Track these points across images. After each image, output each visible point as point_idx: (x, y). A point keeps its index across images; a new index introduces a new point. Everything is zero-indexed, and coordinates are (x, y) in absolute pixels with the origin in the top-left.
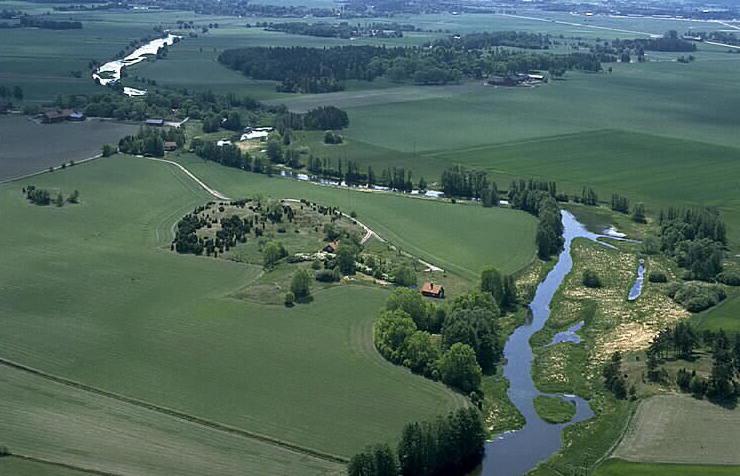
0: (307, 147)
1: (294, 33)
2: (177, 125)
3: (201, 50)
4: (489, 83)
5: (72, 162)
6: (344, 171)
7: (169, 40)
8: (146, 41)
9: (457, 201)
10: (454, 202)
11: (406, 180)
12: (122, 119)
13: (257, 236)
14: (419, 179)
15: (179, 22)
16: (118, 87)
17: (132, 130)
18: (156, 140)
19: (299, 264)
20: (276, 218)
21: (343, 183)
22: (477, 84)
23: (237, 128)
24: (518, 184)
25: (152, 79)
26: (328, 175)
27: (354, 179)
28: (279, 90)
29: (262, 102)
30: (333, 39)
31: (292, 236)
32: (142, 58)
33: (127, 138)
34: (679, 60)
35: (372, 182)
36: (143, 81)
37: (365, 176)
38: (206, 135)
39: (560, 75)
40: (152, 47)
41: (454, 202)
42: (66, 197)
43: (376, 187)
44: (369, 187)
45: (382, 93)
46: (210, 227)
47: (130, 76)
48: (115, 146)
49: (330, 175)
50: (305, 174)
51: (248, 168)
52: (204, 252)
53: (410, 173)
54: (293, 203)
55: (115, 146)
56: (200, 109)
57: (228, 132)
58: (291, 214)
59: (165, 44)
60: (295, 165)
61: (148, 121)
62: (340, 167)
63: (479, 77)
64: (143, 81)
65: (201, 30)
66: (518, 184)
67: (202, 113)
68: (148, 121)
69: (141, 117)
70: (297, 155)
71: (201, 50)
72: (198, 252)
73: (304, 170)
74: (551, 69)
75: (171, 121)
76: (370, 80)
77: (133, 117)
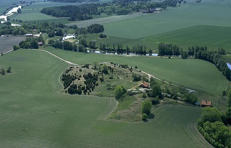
0: (95, 40)
1: (62, 2)
2: (38, 35)
3: (33, 9)
4: (142, 12)
5: (2, 54)
6: (116, 48)
7: (20, 7)
8: (12, 8)
9: (171, 57)
10: (170, 58)
11: (143, 50)
12: (16, 35)
13: (101, 82)
14: (149, 50)
15: (20, 2)
16: (9, 24)
17: (19, 39)
18: (35, 42)
19: (134, 96)
20: (105, 72)
21: (116, 54)
22: (138, 13)
23: (60, 34)
24: (191, 48)
25: (20, 20)
26: (109, 51)
27: (120, 51)
28: (69, 20)
29: (66, 25)
30: (76, 3)
31: (116, 80)
32: (12, 14)
33: (22, 42)
34: (196, 2)
35: (128, 52)
36: (17, 21)
37: (125, 50)
38: (50, 38)
39: (165, 8)
40: (15, 10)
41: (170, 58)
42: (6, 70)
43: (130, 54)
44: (127, 54)
45: (104, 19)
46: (79, 79)
47: (11, 19)
48: (18, 46)
49: (110, 50)
50: (99, 51)
51: (76, 50)
52: (83, 93)
53: (145, 47)
54: (108, 64)
55: (18, 46)
56: (45, 29)
57: (58, 37)
58: (112, 70)
59: (19, 8)
60: (93, 48)
61: (27, 35)
62: (114, 47)
63: (138, 11)
64: (17, 21)
65: (29, 3)
66: (191, 48)
67: (46, 30)
68: (27, 35)
69: (23, 33)
70: (94, 43)
71: (33, 9)
72: (80, 93)
73: (98, 49)
74: (162, 6)
75: (35, 34)
76: (99, 14)
77: (20, 34)
